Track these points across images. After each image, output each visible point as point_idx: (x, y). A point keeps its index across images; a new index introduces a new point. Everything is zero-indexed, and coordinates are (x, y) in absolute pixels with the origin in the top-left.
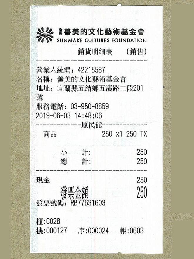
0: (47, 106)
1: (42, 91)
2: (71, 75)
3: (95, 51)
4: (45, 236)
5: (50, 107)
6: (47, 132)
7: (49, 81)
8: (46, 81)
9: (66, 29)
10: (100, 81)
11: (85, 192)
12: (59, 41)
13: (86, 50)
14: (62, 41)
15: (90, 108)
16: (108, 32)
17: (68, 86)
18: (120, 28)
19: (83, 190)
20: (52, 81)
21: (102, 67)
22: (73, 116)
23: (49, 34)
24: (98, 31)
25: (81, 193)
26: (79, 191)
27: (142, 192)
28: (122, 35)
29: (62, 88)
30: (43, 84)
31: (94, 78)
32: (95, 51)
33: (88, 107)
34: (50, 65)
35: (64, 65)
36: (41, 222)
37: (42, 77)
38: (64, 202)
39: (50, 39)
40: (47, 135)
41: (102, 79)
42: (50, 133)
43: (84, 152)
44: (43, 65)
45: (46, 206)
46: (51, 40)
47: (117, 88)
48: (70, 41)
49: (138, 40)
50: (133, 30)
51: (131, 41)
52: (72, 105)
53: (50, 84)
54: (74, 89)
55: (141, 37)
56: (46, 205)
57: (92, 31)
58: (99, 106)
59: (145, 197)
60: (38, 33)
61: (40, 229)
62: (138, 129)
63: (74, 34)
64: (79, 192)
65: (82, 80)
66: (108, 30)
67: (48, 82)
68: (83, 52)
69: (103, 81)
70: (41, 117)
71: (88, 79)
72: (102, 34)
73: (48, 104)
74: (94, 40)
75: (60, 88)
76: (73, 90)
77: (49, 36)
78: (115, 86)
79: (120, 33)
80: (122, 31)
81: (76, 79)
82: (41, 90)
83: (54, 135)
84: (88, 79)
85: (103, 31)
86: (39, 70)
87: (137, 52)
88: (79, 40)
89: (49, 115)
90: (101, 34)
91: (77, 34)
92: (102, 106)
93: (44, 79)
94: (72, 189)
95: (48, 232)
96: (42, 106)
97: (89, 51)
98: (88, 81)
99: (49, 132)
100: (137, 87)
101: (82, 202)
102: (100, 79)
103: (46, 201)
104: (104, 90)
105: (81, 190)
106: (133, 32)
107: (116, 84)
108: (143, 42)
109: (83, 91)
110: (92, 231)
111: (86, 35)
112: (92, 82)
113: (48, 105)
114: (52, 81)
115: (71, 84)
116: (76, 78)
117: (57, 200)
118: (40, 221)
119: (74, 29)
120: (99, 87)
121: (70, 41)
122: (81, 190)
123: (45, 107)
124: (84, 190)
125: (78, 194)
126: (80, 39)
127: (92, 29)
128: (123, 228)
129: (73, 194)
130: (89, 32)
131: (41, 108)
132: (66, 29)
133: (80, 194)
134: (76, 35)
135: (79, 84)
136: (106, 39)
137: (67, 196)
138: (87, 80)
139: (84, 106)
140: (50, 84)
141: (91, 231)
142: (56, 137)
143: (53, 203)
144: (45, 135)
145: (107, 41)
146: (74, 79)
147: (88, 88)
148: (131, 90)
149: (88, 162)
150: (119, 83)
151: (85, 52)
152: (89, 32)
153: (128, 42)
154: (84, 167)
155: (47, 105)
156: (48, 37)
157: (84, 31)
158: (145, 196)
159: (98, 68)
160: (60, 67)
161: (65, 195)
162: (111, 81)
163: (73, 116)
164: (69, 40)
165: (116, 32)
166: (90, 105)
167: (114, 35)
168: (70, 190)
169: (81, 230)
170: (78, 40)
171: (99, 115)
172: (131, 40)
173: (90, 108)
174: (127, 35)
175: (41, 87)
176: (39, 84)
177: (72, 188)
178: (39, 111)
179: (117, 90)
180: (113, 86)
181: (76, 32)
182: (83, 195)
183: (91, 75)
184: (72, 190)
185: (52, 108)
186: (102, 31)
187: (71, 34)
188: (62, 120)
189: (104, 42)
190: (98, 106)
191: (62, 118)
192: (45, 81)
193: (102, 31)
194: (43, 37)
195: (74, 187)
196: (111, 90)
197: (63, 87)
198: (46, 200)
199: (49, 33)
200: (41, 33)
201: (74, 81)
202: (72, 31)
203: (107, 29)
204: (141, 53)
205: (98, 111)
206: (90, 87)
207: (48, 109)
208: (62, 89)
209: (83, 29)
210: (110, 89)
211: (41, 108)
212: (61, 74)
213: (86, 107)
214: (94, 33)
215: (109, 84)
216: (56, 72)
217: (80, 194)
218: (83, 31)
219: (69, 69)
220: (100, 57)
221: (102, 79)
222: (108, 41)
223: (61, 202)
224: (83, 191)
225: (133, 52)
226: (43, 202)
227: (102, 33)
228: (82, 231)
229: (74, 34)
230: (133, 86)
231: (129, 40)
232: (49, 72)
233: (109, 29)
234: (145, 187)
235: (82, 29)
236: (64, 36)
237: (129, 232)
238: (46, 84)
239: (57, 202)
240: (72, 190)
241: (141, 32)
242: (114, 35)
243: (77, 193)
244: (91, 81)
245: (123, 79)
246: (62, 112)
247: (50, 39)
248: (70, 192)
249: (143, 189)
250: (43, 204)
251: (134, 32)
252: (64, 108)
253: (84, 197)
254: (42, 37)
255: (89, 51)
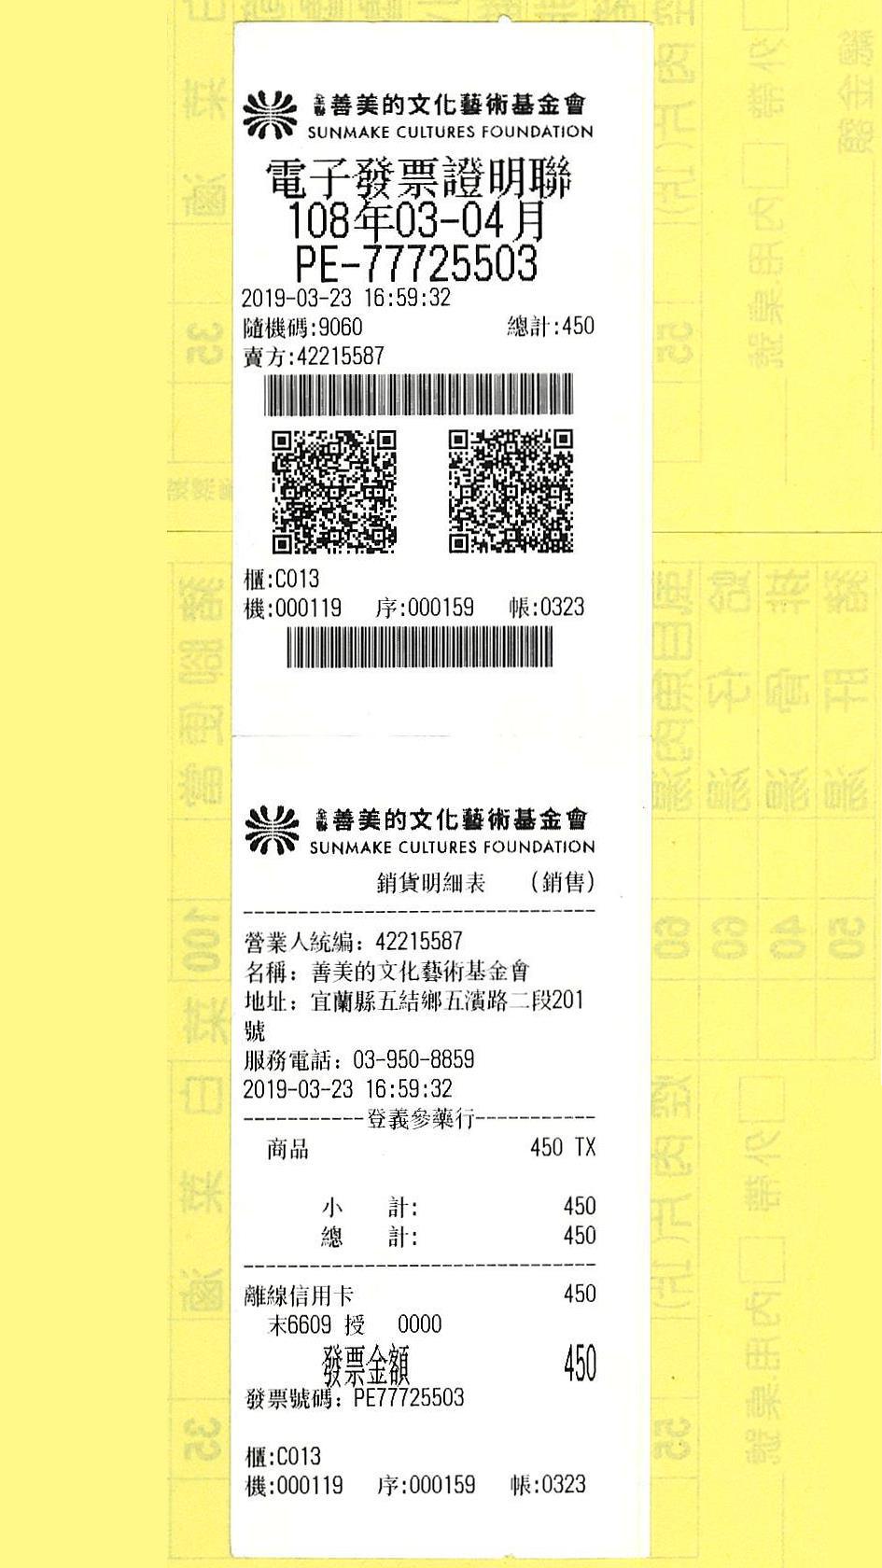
0: (277, 1059)
1: (263, 1009)
2: (353, 958)
3: (431, 882)
4: (275, 1504)
5: (289, 1062)
6: (278, 1143)
7: (283, 977)
8: (276, 977)
9: (337, 95)
10: (447, 977)
11: (398, 1363)
12: (316, 848)
13: (403, 876)
14: (323, 134)
15: (414, 1063)
16: (472, 821)
17: (346, 992)
18: (509, 92)
19: (392, 1356)
20: (293, 978)
21: (452, 933)
22: (361, 1089)
23: (283, 112)
24: (438, 102)
25: (388, 1367)
26: (380, 1360)
27: (581, 1362)
28: (515, 113)
29: (325, 1002)
30: (264, 988)
31: (427, 967)
32: (431, 882)
33: (409, 1062)
34: (288, 927)
35: (331, 925)
36: (259, 580)
37: (261, 965)
38: (334, 1395)
39: (288, 843)
40: (277, 1152)
41: (452, 972)
42: (289, 1147)
43: (398, 1208)
44: (266, 926)
45: (277, 1408)
46: (289, 132)
47: (502, 998)
48: (352, 848)
49: (568, 847)
50: (548, 99)
51: (547, 848)
52: (359, 1054)
53: (288, 989)
54: (362, 1003)
55: (577, 834)
56: (276, 1405)
57: (420, 103)
58: (445, 1058)
59: (591, 1379)
60: (248, 824)
61: (257, 602)
62: (568, 1131)
63: (361, 111)
64: (381, 1365)
65: (388, 975)
66: (471, 97)
67: (282, 981)
68: (394, 886)
69: (457, 977)
70: (258, 303)
71: (407, 970)
72: (452, 110)
73: (281, 1054)
74: (426, 132)
75: (319, 1003)
76: (360, 1006)
77: (283, 832)
78: (493, 995)
79: (509, 107)
80: (517, 817)
81: (371, 971)
82: (260, 1007)
83: (301, 1153)
84: (407, 970)
85: (456, 816)
86: (254, 941)
87: (564, 882)
88: (381, 847)
89: (283, 297)
90: (447, 113)
91: (374, 827)
92: (453, 1057)
93: (270, 971)
94: (357, 1353)
95: (281, 612)
96: (262, 1059)
97: (413, 880)
98: (407, 977)
99: (284, 1143)
100: (562, 995)
101: (389, 1394)
102: (446, 970)
103: (276, 1393)
104: (460, 1007)
105: (388, 1358)
106: (549, 106)
107: (497, 986)
108: (583, 136)
109: (392, 1009)
110: (425, 1485)
111: (401, 113)
112: (422, 980)
113: (280, 1056)
114: (293, 978)
115: (353, 987)
116: (370, 969)
117: (311, 1388)
118: (256, 1457)
119: (363, 96)
120: (444, 999)
121: (352, 850)
122: (388, 1358)
123: (271, 1062)
124: (396, 1357)
125: (377, 1370)
126: (383, 844)
127: (420, 95)
128: (518, 599)
129: (360, 1369)
130: (409, 106)
131: (258, 1066)
132: (337, 95)
133: (383, 1369)
134: (370, 829)
135: (379, 986)
136: (465, 129)
137: (343, 1377)
138: (404, 975)
139: (395, 1059)
140: (288, 989)
141: (420, 1486)
142: (306, 1157)
143: (299, 1400)
144: (272, 1151)
145: (470, 851)
146: (365, 970)
147: (410, 1003)
148: (545, 1005)
149: (408, 1240)
150: (507, 985)
151: (399, 884)
152: (411, 821)
153: (533, 136)
154: (396, 1255)
155: (277, 1056)
156: (281, 837)
157: (392, 102)
158: (591, 1376)
159: (439, 936)
160: (320, 934)
161: (338, 1372)
162: (481, 977)
163: (361, 1089)
164: (347, 130)
165: (497, 104)
166: (414, 1054)
167: (492, 828)
168: (351, 1358)
169: (387, 1485)
170: (374, 132)
171: (443, 1089)
172: (542, 132)
173: (414, 1063)
174: (531, 113)
175: (258, 998)
176: (253, 988)
177: (359, 1351)
178: (254, 1076)
179: (501, 1006)
180: (487, 994)
181: (369, 820)
182: (394, 1374)
183: (419, 958)
184: (359, 1358)
185: (293, 1066)
186: (452, 816)
187: (356, 825)
188: (325, 1104)
189: (459, 137)
190: (441, 1058)
191: (325, 1096)
192: (273, 979)
193: (452, 816)
194: (267, 838)
195: (363, 1348)
196: (482, 1008)
197: (328, 998)
198: (278, 1388)
199: (284, 109)
200: (261, 825)
201: (363, 979)
202: (356, 816)
203: (468, 95)
204: (578, 888)
205: (442, 1073)
206: (415, 997)
207: (283, 1070)
208: (325, 1005)
209: (392, 96)
210: (477, 1003)
211: (261, 1066)
212: (322, 957)
213: (403, 1062)
214: (425, 108)
215: (475, 986)
216: (306, 950)
217: (383, 1369)
218: (392, 101)
219: (348, 940)
220: (447, 899)
221: (453, 971)
222: (473, 850)
223: (324, 1397)
224: (394, 1359)
225: (551, 882)
226: (267, 1398)
227: (450, 110)
228: (390, 1487)
229: (361, 111)
230: (551, 994)
231: (538, 847)
232: (283, 948)
233: (477, 810)
234: (591, 1346)
235: (389, 812)
236: (332, 835)
237: (539, 612)
238: (276, 988)
239: (311, 1396)
240: (359, 1358)
241: (575, 105)
242: (492, 828)
243: (373, 1365)
244: (418, 979)
245: (520, 970)
246: (325, 1077)
247: (287, 842)
248: (351, 1363)
249: (583, 1353)
250: (266, 1403)
251: (554, 818)
252: (333, 1064)
253: (396, 1381)
254: (260, 123)
255: (413, 880)
